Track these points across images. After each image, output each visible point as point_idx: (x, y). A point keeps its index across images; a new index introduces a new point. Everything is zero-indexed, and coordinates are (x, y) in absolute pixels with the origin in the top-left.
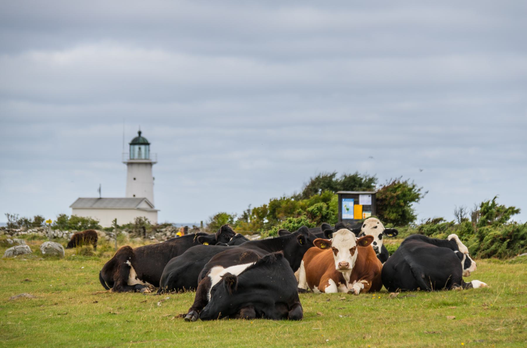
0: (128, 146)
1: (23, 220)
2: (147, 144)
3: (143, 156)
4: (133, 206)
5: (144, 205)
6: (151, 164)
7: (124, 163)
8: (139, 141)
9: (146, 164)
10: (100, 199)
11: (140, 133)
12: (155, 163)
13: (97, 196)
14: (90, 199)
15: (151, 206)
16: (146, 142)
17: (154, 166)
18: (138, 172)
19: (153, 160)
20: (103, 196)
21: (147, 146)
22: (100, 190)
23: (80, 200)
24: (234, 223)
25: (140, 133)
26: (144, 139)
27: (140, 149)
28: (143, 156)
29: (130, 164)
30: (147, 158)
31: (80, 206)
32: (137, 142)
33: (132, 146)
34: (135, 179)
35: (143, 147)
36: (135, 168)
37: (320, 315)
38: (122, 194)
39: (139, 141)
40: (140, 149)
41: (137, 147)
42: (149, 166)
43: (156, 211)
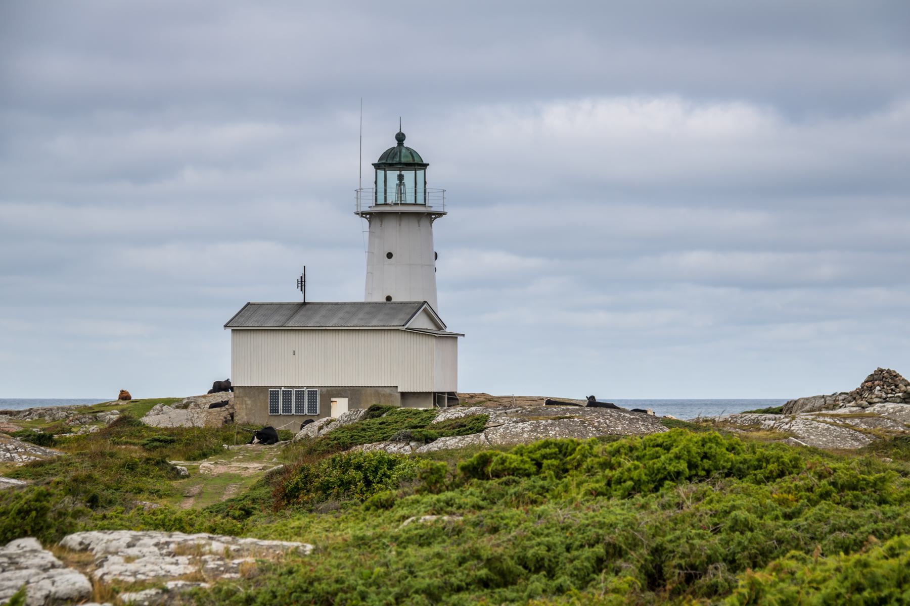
0: (373, 169)
2: (424, 166)
3: (392, 198)
4: (396, 323)
5: (420, 322)
6: (431, 216)
7: (363, 214)
8: (399, 160)
9: (418, 215)
10: (305, 304)
11: (400, 138)
12: (440, 214)
13: (297, 297)
14: (279, 307)
15: (439, 325)
16: (417, 160)
17: (437, 222)
18: (396, 235)
19: (434, 206)
21: (420, 173)
24: (197, 568)
25: (400, 138)
26: (412, 153)
27: (401, 178)
28: (391, 199)
30: (420, 200)
31: (251, 323)
32: (397, 160)
33: (381, 173)
34: (390, 255)
35: (409, 175)
38: (355, 290)
39: (399, 160)
40: (401, 178)
41: (393, 175)
42: (424, 222)
43: (453, 337)
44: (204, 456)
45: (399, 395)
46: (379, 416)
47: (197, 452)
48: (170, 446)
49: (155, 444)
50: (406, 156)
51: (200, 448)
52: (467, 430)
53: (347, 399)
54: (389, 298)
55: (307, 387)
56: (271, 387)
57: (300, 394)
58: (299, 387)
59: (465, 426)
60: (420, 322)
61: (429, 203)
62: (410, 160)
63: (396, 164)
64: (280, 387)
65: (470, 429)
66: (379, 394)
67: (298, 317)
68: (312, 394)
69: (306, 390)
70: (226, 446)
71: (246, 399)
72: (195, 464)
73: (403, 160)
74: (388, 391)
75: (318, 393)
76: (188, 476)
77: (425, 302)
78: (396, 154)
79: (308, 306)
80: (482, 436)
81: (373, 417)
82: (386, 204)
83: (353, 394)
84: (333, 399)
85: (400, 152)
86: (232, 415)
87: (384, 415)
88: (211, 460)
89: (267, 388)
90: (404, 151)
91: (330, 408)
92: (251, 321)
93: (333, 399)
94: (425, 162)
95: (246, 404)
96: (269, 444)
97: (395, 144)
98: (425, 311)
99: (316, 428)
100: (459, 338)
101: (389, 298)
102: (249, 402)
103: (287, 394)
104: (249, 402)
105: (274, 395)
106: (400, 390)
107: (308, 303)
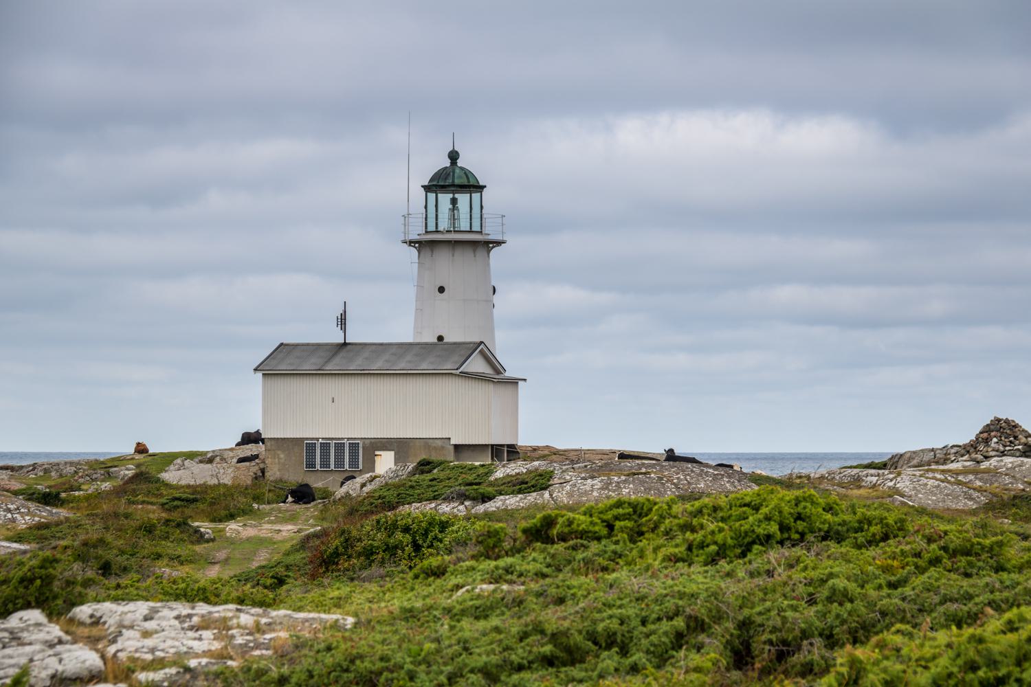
0: (422, 191)
1: (347, 443)
2: (480, 188)
3: (444, 224)
4: (448, 366)
5: (476, 365)
6: (489, 245)
7: (411, 243)
8: (452, 181)
9: (474, 244)
10: (345, 344)
11: (454, 156)
12: (498, 243)
15: (497, 369)
16: (472, 182)
17: (495, 252)
18: (447, 266)
20: (355, 335)
21: (476, 196)
22: (342, 321)
23: (283, 349)
25: (454, 156)
26: (467, 173)
28: (444, 224)
29: (426, 245)
30: (476, 227)
32: (449, 181)
33: (432, 196)
34: (441, 290)
35: (463, 199)
36: (443, 256)
37: (597, 613)
38: (402, 330)
39: (452, 181)
41: (445, 199)
42: (481, 252)
43: (514, 382)
44: (231, 517)
45: (452, 448)
46: (430, 471)
47: (223, 513)
48: (192, 506)
49: (176, 503)
50: (460, 177)
51: (227, 508)
52: (529, 487)
53: (392, 453)
54: (440, 338)
55: (348, 439)
56: (307, 439)
57: (340, 447)
58: (339, 439)
59: (527, 483)
60: (476, 365)
61: (486, 230)
62: (464, 181)
63: (448, 186)
64: (317, 439)
65: (533, 486)
66: (429, 446)
67: (338, 360)
68: (354, 447)
69: (347, 443)
70: (256, 506)
71: (279, 452)
72: (221, 526)
73: (457, 182)
74: (439, 443)
75: (361, 445)
76: (213, 540)
77: (482, 342)
78: (449, 174)
79: (349, 347)
80: (547, 494)
81: (422, 472)
82: (437, 232)
83: (400, 446)
84: (377, 453)
85: (454, 172)
86: (263, 471)
87: (435, 471)
88: (238, 522)
89: (302, 439)
90: (457, 171)
91: (374, 462)
92: (285, 364)
93: (377, 453)
94: (481, 184)
95: (279, 458)
96: (305, 503)
97: (447, 163)
98: (482, 352)
99: (358, 486)
100: (520, 382)
101: (440, 338)
102: (282, 456)
103: (325, 447)
104: (282, 456)
105: (311, 448)
106: (453, 442)
107: (349, 344)
